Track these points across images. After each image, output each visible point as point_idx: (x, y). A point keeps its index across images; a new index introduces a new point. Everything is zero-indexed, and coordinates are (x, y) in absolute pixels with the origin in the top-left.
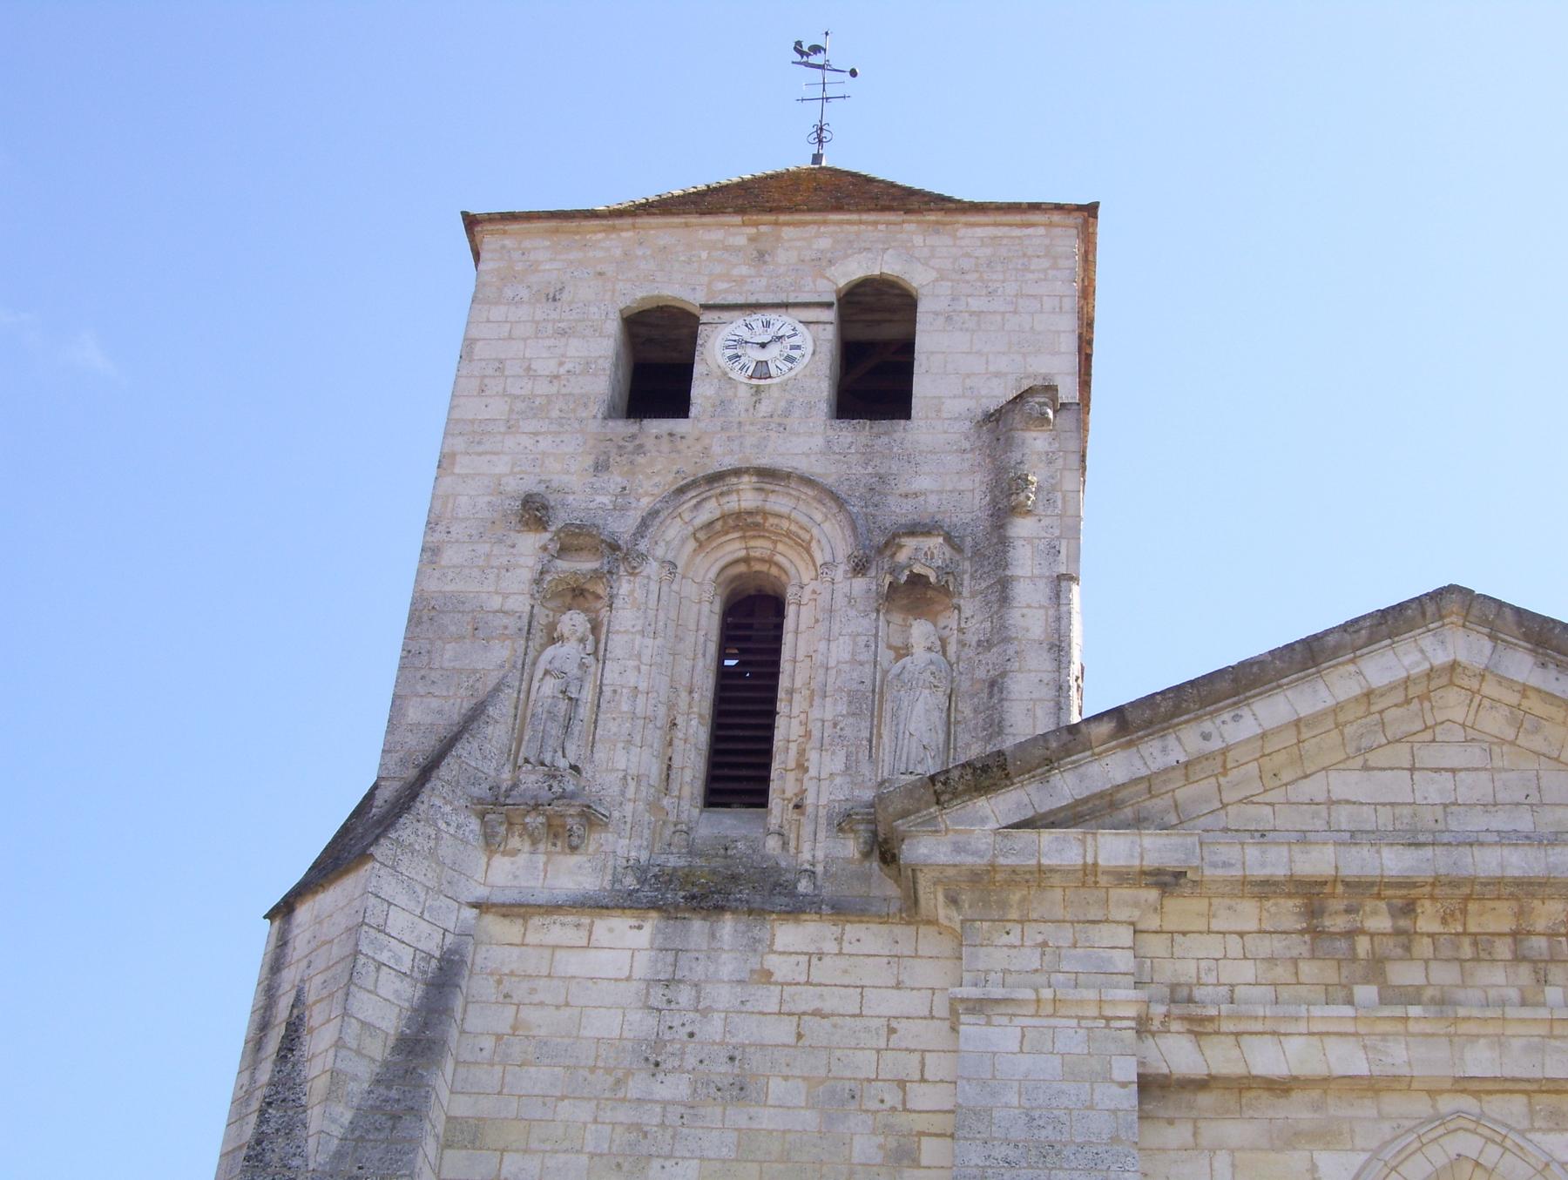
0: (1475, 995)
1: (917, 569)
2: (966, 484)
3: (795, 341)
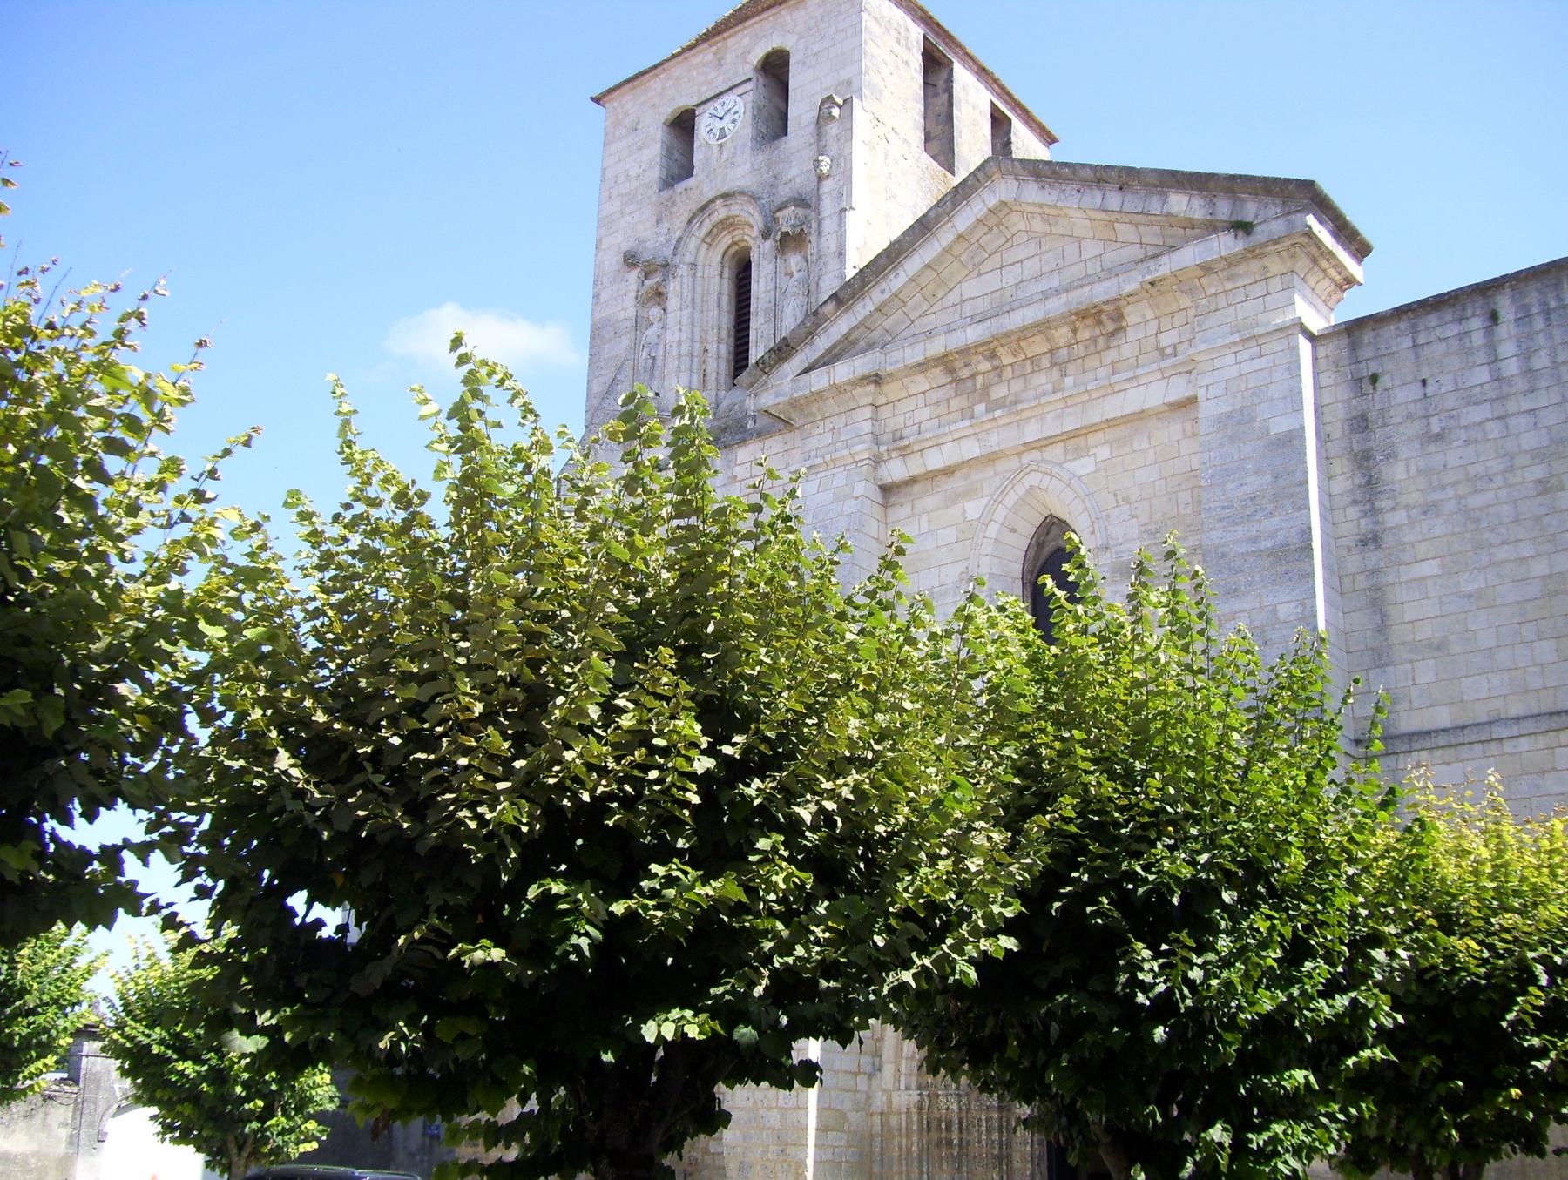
0: (1031, 394)
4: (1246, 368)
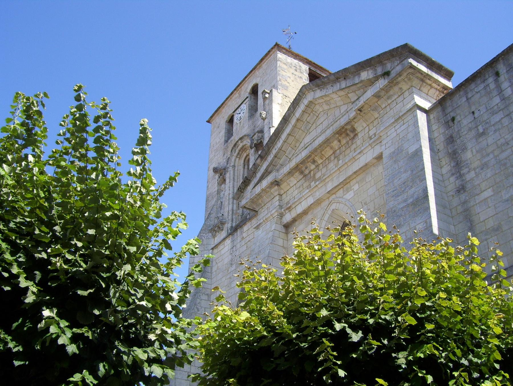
4: (399, 131)
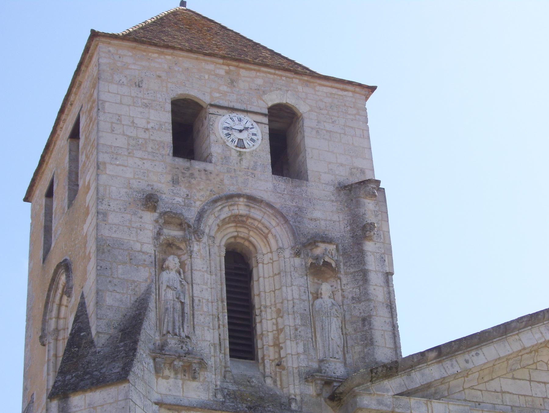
1: (327, 259)
2: (335, 218)
3: (254, 131)
